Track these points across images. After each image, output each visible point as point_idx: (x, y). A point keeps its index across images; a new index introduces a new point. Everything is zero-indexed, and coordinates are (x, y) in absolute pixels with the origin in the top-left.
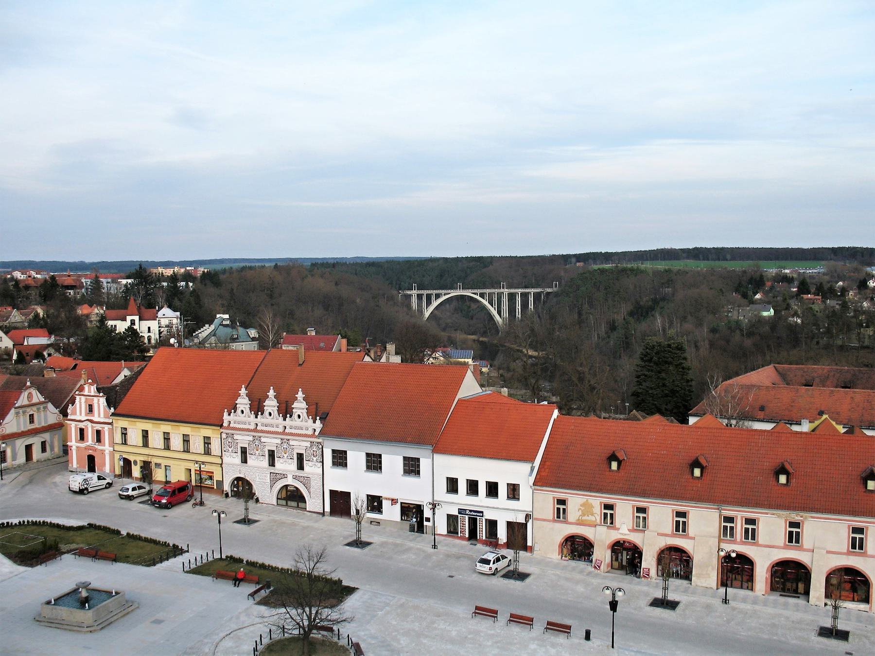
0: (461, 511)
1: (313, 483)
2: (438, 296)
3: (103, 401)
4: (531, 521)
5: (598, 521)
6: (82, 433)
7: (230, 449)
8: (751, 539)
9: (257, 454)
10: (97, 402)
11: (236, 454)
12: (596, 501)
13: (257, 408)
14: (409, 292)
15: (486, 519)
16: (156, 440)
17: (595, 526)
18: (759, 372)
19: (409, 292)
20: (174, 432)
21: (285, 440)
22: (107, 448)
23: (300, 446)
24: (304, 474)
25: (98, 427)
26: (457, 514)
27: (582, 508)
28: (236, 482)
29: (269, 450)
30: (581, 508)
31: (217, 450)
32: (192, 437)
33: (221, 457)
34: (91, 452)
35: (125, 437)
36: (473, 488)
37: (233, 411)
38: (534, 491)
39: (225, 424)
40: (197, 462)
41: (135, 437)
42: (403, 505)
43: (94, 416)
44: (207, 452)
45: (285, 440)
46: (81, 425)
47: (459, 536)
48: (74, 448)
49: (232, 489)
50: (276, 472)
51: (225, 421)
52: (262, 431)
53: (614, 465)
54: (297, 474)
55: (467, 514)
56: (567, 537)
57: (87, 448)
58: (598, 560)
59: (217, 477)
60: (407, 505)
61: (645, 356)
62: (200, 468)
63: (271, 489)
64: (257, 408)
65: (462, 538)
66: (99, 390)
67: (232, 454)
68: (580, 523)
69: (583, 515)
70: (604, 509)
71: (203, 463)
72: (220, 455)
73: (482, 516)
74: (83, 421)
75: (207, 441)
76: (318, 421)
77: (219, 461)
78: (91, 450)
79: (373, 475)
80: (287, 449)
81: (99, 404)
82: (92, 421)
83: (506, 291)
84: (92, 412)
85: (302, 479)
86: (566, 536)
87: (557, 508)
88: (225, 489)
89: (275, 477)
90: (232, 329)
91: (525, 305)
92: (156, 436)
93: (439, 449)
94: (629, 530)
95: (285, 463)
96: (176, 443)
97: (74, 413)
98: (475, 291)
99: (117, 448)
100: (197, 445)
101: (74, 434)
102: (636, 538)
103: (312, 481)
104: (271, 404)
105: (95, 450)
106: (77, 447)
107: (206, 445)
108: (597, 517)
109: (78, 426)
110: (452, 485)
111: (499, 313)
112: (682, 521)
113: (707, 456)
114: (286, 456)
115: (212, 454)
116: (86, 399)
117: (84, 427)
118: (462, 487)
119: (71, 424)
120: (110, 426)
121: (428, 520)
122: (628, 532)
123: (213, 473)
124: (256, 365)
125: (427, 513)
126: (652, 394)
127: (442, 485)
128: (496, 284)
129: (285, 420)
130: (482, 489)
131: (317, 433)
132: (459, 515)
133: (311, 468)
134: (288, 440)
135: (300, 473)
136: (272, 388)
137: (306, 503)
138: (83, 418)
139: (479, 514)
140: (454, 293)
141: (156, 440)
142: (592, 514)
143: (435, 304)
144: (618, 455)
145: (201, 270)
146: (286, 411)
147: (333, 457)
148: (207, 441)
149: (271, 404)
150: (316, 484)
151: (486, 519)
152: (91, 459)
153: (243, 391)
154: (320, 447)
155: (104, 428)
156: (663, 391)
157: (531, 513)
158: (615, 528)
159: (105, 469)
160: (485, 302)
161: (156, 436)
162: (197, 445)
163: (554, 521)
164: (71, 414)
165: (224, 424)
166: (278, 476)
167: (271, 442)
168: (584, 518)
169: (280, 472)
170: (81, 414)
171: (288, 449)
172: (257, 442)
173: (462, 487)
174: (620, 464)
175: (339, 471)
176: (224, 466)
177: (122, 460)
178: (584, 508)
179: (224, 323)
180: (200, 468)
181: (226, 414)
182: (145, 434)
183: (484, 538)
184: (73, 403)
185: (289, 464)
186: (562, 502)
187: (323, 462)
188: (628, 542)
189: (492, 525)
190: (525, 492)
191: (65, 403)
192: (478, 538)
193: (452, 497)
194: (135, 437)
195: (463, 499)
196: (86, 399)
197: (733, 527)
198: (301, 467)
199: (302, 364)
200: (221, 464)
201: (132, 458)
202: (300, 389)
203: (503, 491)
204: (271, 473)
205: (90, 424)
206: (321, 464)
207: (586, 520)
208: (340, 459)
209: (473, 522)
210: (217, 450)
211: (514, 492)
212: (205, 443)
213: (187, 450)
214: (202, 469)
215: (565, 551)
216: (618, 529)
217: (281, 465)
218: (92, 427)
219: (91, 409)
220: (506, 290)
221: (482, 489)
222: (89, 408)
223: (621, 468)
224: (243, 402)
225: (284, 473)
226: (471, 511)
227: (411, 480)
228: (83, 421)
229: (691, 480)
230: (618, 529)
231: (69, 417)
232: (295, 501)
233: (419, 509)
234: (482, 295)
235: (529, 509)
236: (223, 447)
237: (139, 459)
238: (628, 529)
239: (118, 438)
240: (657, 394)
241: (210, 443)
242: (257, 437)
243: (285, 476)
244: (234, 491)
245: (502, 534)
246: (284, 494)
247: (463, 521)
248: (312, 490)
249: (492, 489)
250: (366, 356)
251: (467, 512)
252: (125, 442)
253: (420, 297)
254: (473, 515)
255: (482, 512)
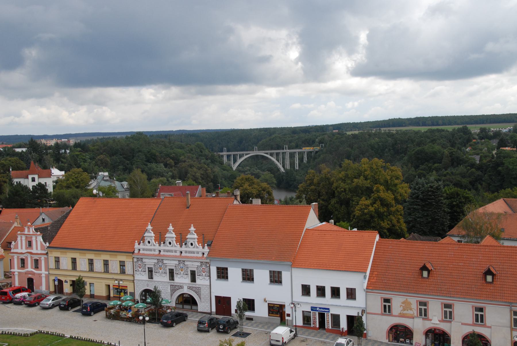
0: (313, 309)
1: (202, 292)
2: (241, 156)
3: (40, 239)
4: (365, 315)
5: (416, 314)
6: (23, 262)
7: (140, 270)
8: (481, 322)
9: (161, 272)
10: (35, 239)
11: (145, 273)
12: (413, 301)
13: (161, 239)
14: (221, 154)
15: (331, 314)
16: (83, 264)
17: (413, 318)
18: (494, 204)
19: (221, 154)
20: (62, 256)
21: (182, 261)
22: (43, 272)
23: (193, 266)
24: (196, 285)
25: (36, 257)
26: (310, 310)
27: (403, 305)
28: (144, 293)
29: (169, 269)
30: (402, 305)
31: (130, 271)
32: (111, 261)
33: (133, 276)
34: (30, 276)
35: (74, 265)
36: (321, 291)
37: (142, 242)
38: (367, 293)
39: (136, 251)
40: (116, 280)
41: (66, 263)
42: (269, 305)
43: (32, 249)
44: (123, 272)
45: (182, 261)
46: (22, 256)
47: (312, 326)
48: (16, 273)
49: (141, 298)
50: (175, 284)
51: (136, 249)
52: (164, 256)
53: (425, 274)
54: (191, 285)
55: (318, 311)
56: (392, 326)
57: (26, 273)
58: (418, 343)
59: (130, 290)
60: (272, 305)
61: (414, 194)
62: (119, 284)
63: (171, 297)
64: (161, 239)
65: (314, 328)
66: (36, 230)
67: (141, 273)
68: (401, 316)
69: (404, 310)
70: (444, 308)
71: (121, 280)
72: (132, 273)
73: (329, 312)
74: (23, 254)
75: (122, 265)
76: (206, 247)
77: (131, 278)
78: (30, 274)
79: (248, 285)
80: (183, 267)
81: (36, 241)
82: (31, 253)
83: (288, 151)
84: (31, 246)
85: (194, 289)
86: (392, 325)
87: (384, 305)
88: (136, 299)
89: (174, 289)
90: (111, 182)
91: (301, 160)
92: (82, 262)
93: (295, 264)
94: (439, 321)
95: (181, 278)
96: (99, 266)
97: (16, 247)
98: (267, 152)
99: (51, 272)
100: (114, 267)
101: (16, 262)
102: (444, 327)
103: (202, 290)
104: (171, 236)
105: (34, 274)
106: (19, 273)
107: (122, 267)
108: (415, 312)
109: (20, 257)
110: (306, 290)
111: (283, 166)
112: (449, 311)
113: (495, 266)
114: (182, 272)
115: (110, 272)
116: (26, 237)
117: (24, 258)
118: (313, 291)
119: (14, 256)
120: (46, 256)
121: (288, 315)
122: (438, 322)
123: (127, 287)
124: (155, 208)
125: (288, 310)
126: (419, 221)
127: (299, 290)
128: (279, 147)
129: (182, 247)
130: (328, 292)
131: (205, 255)
132: (312, 312)
133: (200, 281)
134: (184, 261)
135: (193, 285)
136: (192, 225)
137: (197, 306)
138: (24, 251)
139: (326, 310)
140: (252, 154)
141: (83, 264)
142: (411, 309)
143: (239, 161)
144: (428, 266)
145: (72, 142)
146: (182, 240)
147: (218, 272)
148: (122, 265)
149: (171, 236)
150: (204, 292)
151: (331, 314)
152: (30, 281)
153: (149, 227)
154: (208, 265)
155: (41, 258)
156: (427, 219)
157: (365, 309)
158: (428, 319)
159: (42, 288)
160: (274, 159)
161: (82, 262)
162: (114, 267)
163: (382, 314)
164: (14, 249)
165: (135, 251)
166: (177, 287)
167: (171, 264)
168: (405, 312)
169: (178, 284)
170: (22, 248)
171: (184, 267)
172: (182, 265)
173: (313, 291)
174: (429, 271)
175: (222, 282)
176: (135, 281)
177: (57, 280)
178: (404, 305)
179: (105, 178)
180: (119, 284)
181: (136, 244)
182: (74, 261)
183: (330, 328)
184: (16, 240)
185: (185, 278)
186: (387, 300)
187: (210, 276)
188: (438, 330)
189: (336, 319)
190: (360, 294)
191: (3, 240)
192: (326, 328)
193: (306, 299)
194: (66, 263)
195: (314, 299)
196: (26, 237)
197: (451, 311)
198: (193, 280)
199: (189, 207)
200: (133, 281)
201: (63, 279)
202: (171, 224)
203: (343, 293)
204: (171, 285)
205: (29, 256)
206: (209, 277)
207: (406, 314)
208: (223, 274)
209: (322, 316)
210: (130, 271)
211: (351, 294)
212: (120, 266)
213: (107, 271)
214: (120, 285)
215: (391, 336)
216: (431, 320)
217: (178, 280)
218: (31, 257)
219: (30, 244)
220: (289, 151)
221: (328, 292)
222: (29, 244)
223: (430, 275)
224: (150, 235)
225: (181, 285)
226: (320, 308)
227: (276, 287)
228: (23, 254)
229: (485, 284)
230: (431, 320)
231: (12, 251)
232: (189, 305)
233: (282, 307)
234: (271, 155)
235: (363, 306)
236: (134, 268)
237: (69, 279)
238: (438, 320)
239: (52, 265)
240: (423, 221)
241: (125, 266)
242: (160, 260)
243: (181, 287)
244: (142, 299)
245: (344, 324)
246: (181, 300)
247: (314, 315)
248: (202, 296)
249: (336, 292)
250: (235, 200)
251: (318, 309)
252: (58, 268)
253: (228, 156)
254: (322, 311)
255: (328, 309)
